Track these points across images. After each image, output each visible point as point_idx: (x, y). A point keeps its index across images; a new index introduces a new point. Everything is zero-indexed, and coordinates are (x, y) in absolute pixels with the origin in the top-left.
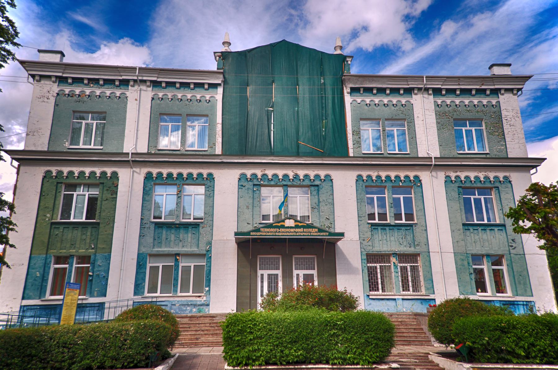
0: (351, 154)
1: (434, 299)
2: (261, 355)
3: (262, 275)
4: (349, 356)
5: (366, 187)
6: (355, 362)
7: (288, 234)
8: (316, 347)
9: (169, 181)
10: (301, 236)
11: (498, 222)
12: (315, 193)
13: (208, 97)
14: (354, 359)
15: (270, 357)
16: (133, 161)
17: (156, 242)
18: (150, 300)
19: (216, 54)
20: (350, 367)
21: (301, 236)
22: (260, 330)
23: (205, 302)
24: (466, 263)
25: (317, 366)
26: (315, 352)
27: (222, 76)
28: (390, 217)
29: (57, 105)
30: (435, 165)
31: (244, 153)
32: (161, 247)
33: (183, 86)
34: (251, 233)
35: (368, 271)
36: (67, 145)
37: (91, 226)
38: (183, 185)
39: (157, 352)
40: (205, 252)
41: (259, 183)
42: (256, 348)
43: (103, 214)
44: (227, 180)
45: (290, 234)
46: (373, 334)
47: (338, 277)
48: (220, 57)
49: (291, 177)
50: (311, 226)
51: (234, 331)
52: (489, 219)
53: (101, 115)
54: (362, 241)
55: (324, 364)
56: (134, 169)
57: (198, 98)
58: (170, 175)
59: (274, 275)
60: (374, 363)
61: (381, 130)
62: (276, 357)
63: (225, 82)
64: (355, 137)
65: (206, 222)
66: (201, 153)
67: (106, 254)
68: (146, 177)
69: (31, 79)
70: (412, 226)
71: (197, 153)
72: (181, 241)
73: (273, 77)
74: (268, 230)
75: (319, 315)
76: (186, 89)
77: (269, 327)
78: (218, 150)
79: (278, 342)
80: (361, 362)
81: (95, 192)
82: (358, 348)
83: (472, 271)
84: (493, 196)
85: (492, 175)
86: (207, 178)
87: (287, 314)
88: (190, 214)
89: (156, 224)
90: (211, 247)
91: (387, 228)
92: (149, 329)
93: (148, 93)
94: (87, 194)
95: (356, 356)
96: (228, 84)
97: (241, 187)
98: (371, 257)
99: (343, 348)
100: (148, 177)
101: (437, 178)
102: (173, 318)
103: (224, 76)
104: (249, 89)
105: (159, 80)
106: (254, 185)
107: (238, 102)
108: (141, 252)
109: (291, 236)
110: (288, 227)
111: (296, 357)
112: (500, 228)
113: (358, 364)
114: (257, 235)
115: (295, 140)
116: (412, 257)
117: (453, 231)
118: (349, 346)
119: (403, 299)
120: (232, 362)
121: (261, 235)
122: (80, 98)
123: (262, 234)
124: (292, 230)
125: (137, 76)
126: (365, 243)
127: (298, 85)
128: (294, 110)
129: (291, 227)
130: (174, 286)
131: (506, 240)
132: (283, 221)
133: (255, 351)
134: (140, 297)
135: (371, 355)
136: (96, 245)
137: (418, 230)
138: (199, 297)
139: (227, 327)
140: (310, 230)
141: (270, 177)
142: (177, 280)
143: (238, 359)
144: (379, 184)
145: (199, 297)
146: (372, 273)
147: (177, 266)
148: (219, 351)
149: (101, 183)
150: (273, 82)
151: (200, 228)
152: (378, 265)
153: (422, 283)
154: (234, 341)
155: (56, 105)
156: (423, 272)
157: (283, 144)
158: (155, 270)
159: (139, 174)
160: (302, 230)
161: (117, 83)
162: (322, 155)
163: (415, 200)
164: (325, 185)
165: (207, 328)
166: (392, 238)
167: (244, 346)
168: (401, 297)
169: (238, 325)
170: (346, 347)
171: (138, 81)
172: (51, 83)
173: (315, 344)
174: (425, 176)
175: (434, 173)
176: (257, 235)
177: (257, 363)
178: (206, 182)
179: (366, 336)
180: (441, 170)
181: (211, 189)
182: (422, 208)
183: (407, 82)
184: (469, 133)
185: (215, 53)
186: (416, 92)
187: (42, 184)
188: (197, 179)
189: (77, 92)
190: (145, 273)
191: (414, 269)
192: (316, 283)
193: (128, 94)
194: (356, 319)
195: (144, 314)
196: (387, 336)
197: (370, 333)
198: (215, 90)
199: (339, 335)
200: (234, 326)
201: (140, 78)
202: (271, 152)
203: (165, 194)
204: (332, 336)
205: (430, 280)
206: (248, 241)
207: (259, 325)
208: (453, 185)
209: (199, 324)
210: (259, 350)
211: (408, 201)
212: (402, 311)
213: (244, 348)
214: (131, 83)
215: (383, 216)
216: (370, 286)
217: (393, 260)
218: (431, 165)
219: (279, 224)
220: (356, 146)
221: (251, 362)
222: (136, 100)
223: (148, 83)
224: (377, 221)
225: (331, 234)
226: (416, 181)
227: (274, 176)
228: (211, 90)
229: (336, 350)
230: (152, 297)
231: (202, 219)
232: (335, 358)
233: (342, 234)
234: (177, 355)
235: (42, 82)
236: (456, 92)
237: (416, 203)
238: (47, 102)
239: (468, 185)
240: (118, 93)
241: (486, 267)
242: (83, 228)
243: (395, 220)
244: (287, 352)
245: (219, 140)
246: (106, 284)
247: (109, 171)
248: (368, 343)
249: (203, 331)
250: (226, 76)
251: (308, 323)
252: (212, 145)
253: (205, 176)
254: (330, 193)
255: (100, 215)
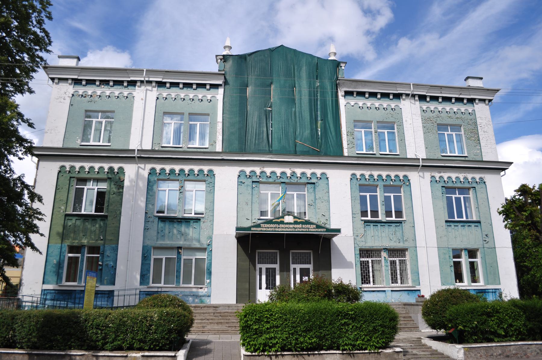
0: (346, 154)
1: (420, 290)
2: (277, 342)
3: (295, 269)
4: (358, 342)
5: (364, 187)
6: (364, 347)
7: (287, 230)
8: (328, 335)
9: (172, 176)
10: (299, 231)
11: (475, 219)
12: (311, 190)
13: (209, 97)
14: (363, 345)
15: (285, 344)
16: (138, 157)
17: (159, 235)
18: (156, 290)
19: (218, 57)
20: (359, 352)
21: (299, 231)
22: (276, 319)
23: (206, 294)
24: (447, 257)
25: (328, 352)
26: (327, 340)
27: (223, 77)
28: (382, 214)
29: (72, 105)
30: (423, 166)
31: (243, 151)
32: (164, 240)
33: (186, 87)
34: (252, 229)
35: (361, 265)
36: (79, 141)
37: (100, 219)
38: (185, 181)
39: (179, 338)
40: (205, 246)
41: (258, 180)
42: (273, 336)
43: (110, 208)
44: (227, 177)
45: (290, 230)
46: (380, 322)
47: (332, 270)
48: (221, 60)
49: (289, 175)
50: (308, 222)
51: (251, 321)
52: (467, 217)
53: (107, 114)
54: (356, 237)
55: (335, 350)
56: (139, 165)
57: (200, 98)
58: (172, 171)
59: (272, 268)
60: (380, 348)
61: (373, 132)
62: (291, 344)
63: (226, 83)
64: (349, 137)
65: (207, 217)
66: (202, 150)
67: (114, 246)
68: (150, 173)
69: (51, 82)
70: (401, 223)
71: (199, 150)
72: (183, 235)
73: (272, 79)
74: (268, 225)
75: (331, 306)
76: (189, 89)
77: (284, 317)
78: (219, 148)
79: (293, 331)
80: (369, 348)
81: (103, 186)
82: (366, 335)
83: (452, 264)
84: (471, 194)
85: (470, 176)
86: (208, 175)
87: (300, 305)
88: (192, 210)
89: (160, 218)
90: (211, 241)
91: (379, 225)
92: (171, 317)
93: (153, 93)
94: (96, 188)
95: (364, 342)
96: (228, 84)
97: (240, 183)
98: (365, 252)
99: (352, 336)
100: (152, 172)
101: (423, 178)
102: (188, 307)
103: (225, 77)
104: (249, 90)
105: (164, 81)
106: (253, 182)
107: (238, 102)
108: (146, 244)
109: (290, 231)
110: (287, 223)
111: (310, 344)
112: (476, 224)
113: (366, 349)
114: (257, 231)
115: (293, 139)
116: (400, 252)
117: (437, 228)
118: (358, 334)
119: (392, 291)
120: (250, 348)
121: (261, 231)
122: (92, 98)
123: (262, 229)
124: (291, 226)
125: (144, 78)
126: (358, 239)
127: (295, 87)
128: (292, 110)
129: (290, 224)
130: (177, 277)
131: (481, 235)
132: (283, 217)
133: (271, 338)
134: (146, 287)
135: (378, 341)
136: (105, 237)
137: (406, 227)
138: (201, 288)
139: (245, 316)
140: (308, 226)
141: (268, 174)
142: (180, 272)
143: (255, 345)
144: (372, 183)
145: (201, 288)
146: (364, 267)
147: (179, 259)
148: (237, 338)
149: (109, 178)
150: (271, 83)
151: (201, 223)
152: (370, 260)
153: (409, 276)
154: (252, 329)
155: (71, 105)
156: (411, 265)
157: (281, 142)
158: (158, 261)
159: (144, 169)
160: (300, 226)
161: (125, 84)
162: (318, 154)
163: (404, 198)
164: (322, 183)
165: (211, 318)
166: (383, 235)
167: (261, 333)
168: (391, 289)
169: (255, 315)
170: (356, 335)
171: (145, 82)
172: (68, 85)
173: (327, 333)
174: (414, 176)
175: (421, 174)
176: (257, 231)
177: (273, 349)
178: (206, 178)
179: (375, 324)
180: (428, 171)
181: (211, 185)
182: (411, 206)
183: (396, 88)
184: (450, 136)
185: (217, 56)
186: (404, 97)
187: (58, 179)
188: (198, 175)
189: (90, 93)
190: (150, 264)
191: (402, 262)
192: (312, 277)
193: (135, 94)
194: (365, 309)
195: (162, 302)
196: (393, 324)
197: (377, 321)
198: (216, 90)
199: (350, 324)
200: (252, 316)
201: (147, 79)
202: (269, 150)
203: (168, 189)
204: (343, 325)
205: (416, 273)
206: (247, 236)
207: (275, 315)
208: (437, 185)
209: (203, 313)
210: (275, 338)
211: (398, 199)
212: (391, 301)
213: (261, 336)
214: (138, 84)
215: (375, 213)
216: (362, 278)
217: (384, 254)
218: (419, 166)
219: (279, 220)
220: (351, 146)
221: (267, 348)
222: (142, 99)
223: (154, 84)
224: (369, 218)
225: (328, 230)
226: (405, 181)
227: (272, 174)
228: (212, 90)
229: (347, 337)
230: (158, 287)
231: (203, 214)
232: (346, 345)
233: (339, 231)
234: (191, 341)
235: (60, 84)
236: (451, 101)
237: (405, 201)
238: (64, 102)
239: (450, 185)
240: (126, 92)
241: (464, 261)
242: (93, 220)
243: (387, 217)
244: (302, 339)
245: (220, 138)
246: (115, 274)
247: (116, 166)
248: (375, 330)
249: (208, 320)
250: (227, 78)
251: (321, 313)
252: (213, 143)
253: (206, 173)
254: (326, 190)
255: (108, 209)
